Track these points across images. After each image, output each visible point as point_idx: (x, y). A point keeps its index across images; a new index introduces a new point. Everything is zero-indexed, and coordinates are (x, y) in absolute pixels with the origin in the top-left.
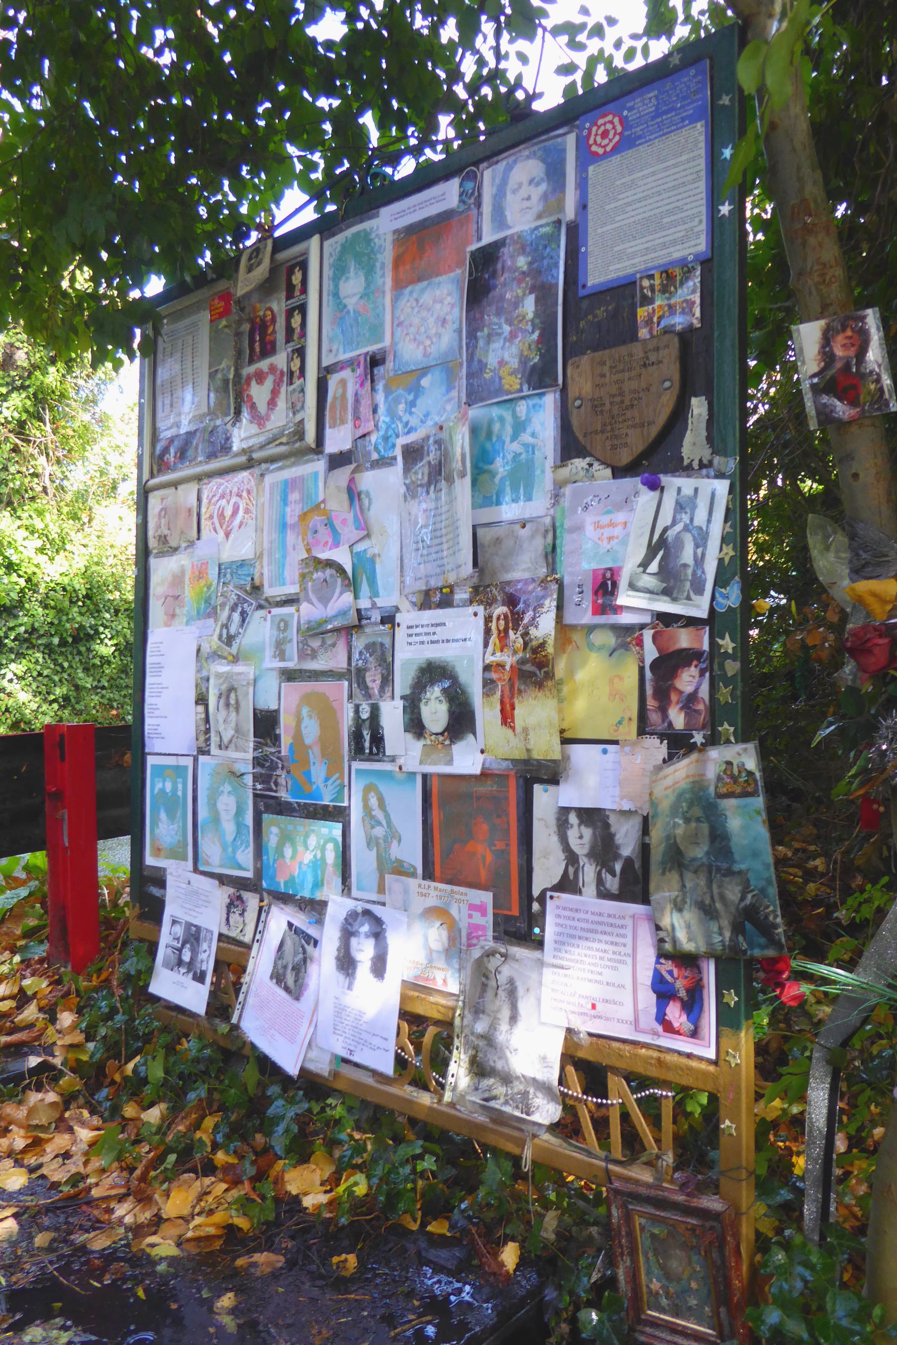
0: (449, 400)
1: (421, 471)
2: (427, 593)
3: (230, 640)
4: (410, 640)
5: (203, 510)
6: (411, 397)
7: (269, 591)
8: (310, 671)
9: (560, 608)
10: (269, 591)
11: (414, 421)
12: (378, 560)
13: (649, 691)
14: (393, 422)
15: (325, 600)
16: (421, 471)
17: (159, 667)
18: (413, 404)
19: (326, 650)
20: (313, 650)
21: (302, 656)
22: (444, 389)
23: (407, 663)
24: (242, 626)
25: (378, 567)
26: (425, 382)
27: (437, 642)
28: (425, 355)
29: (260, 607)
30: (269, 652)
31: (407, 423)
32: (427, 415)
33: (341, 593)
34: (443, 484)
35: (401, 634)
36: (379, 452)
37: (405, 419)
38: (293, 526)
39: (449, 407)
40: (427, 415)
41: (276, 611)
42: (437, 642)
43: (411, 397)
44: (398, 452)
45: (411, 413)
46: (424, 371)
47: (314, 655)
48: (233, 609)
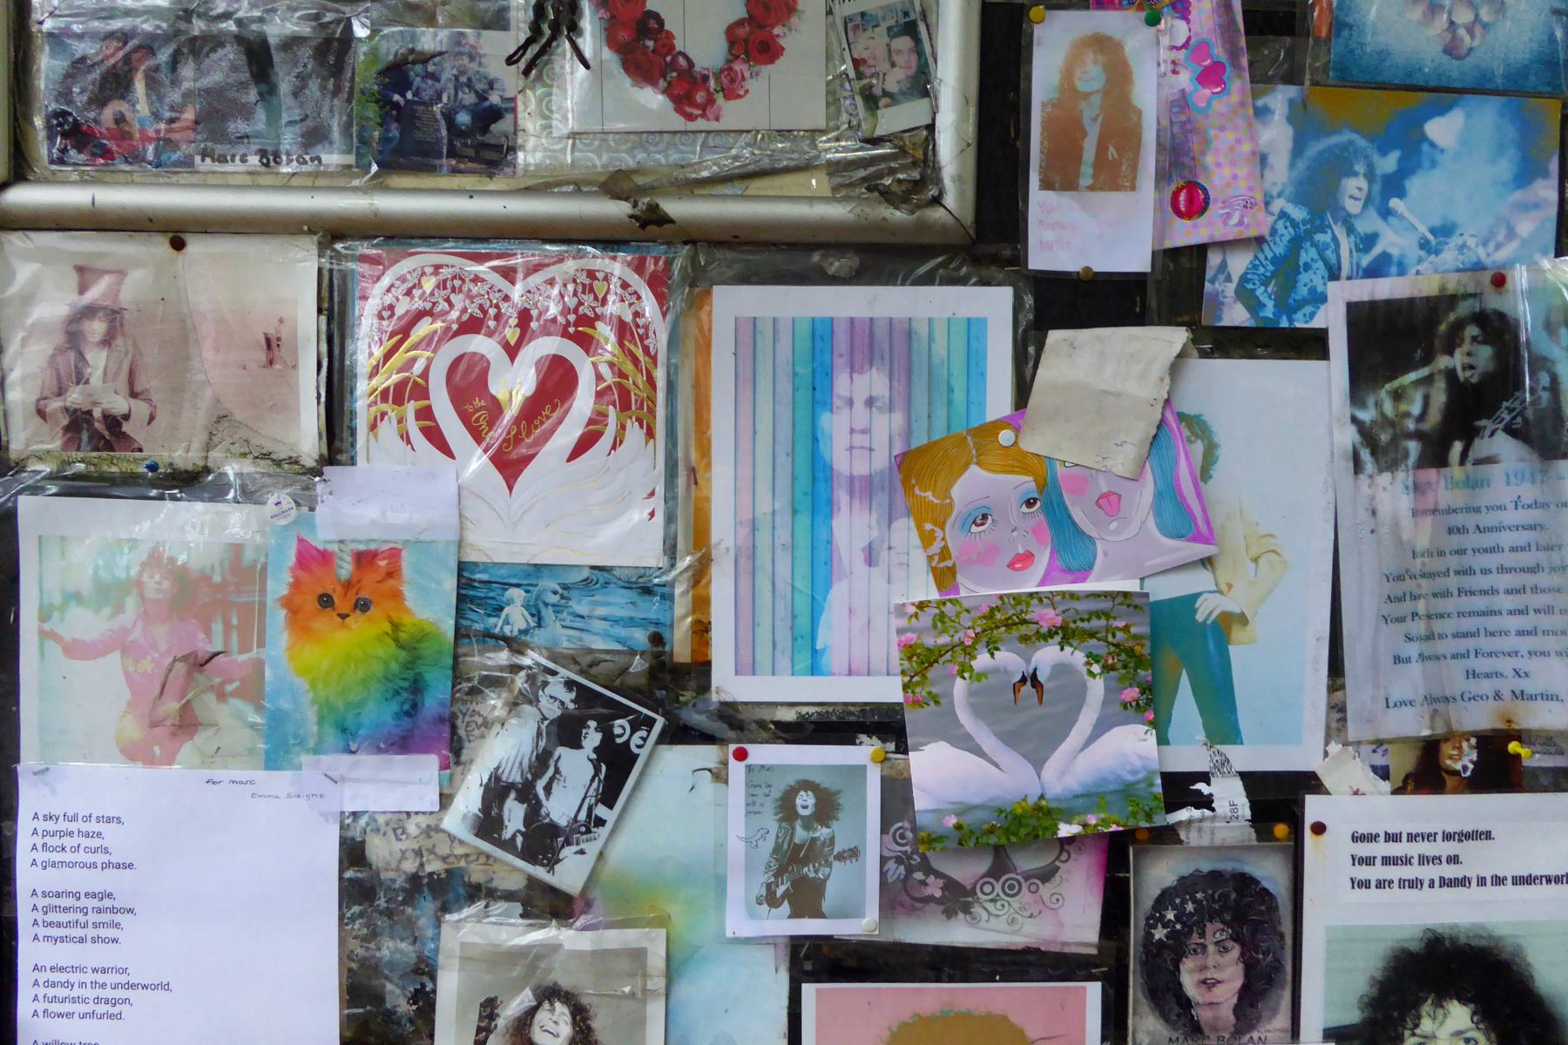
0: (1525, 207)
1: (1418, 397)
2: (1430, 750)
3: (543, 841)
4: (1363, 872)
5: (365, 347)
6: (1388, 163)
7: (730, 683)
8: (938, 950)
9: (1330, 405)
10: (730, 683)
11: (1392, 241)
12: (1237, 633)
13: (1031, 364)
14: (1317, 223)
15: (1036, 745)
16: (1418, 397)
17: (104, 913)
18: (1394, 185)
19: (1013, 891)
20: (952, 886)
21: (895, 899)
22: (1506, 167)
23: (1344, 940)
24: (609, 796)
25: (1238, 654)
26: (1442, 129)
27: (1463, 882)
28: (1451, 50)
29: (680, 734)
30: (740, 889)
31: (1369, 241)
32: (1445, 231)
33: (1101, 727)
34: (1168, 144)
35: (1326, 860)
36: (1254, 306)
37: (1363, 227)
38: (864, 488)
39: (1525, 228)
40: (1445, 231)
41: (762, 754)
42: (1463, 882)
43: (1388, 163)
44: (1332, 319)
45: (1386, 213)
46: (1443, 93)
47: (957, 900)
48: (566, 731)
